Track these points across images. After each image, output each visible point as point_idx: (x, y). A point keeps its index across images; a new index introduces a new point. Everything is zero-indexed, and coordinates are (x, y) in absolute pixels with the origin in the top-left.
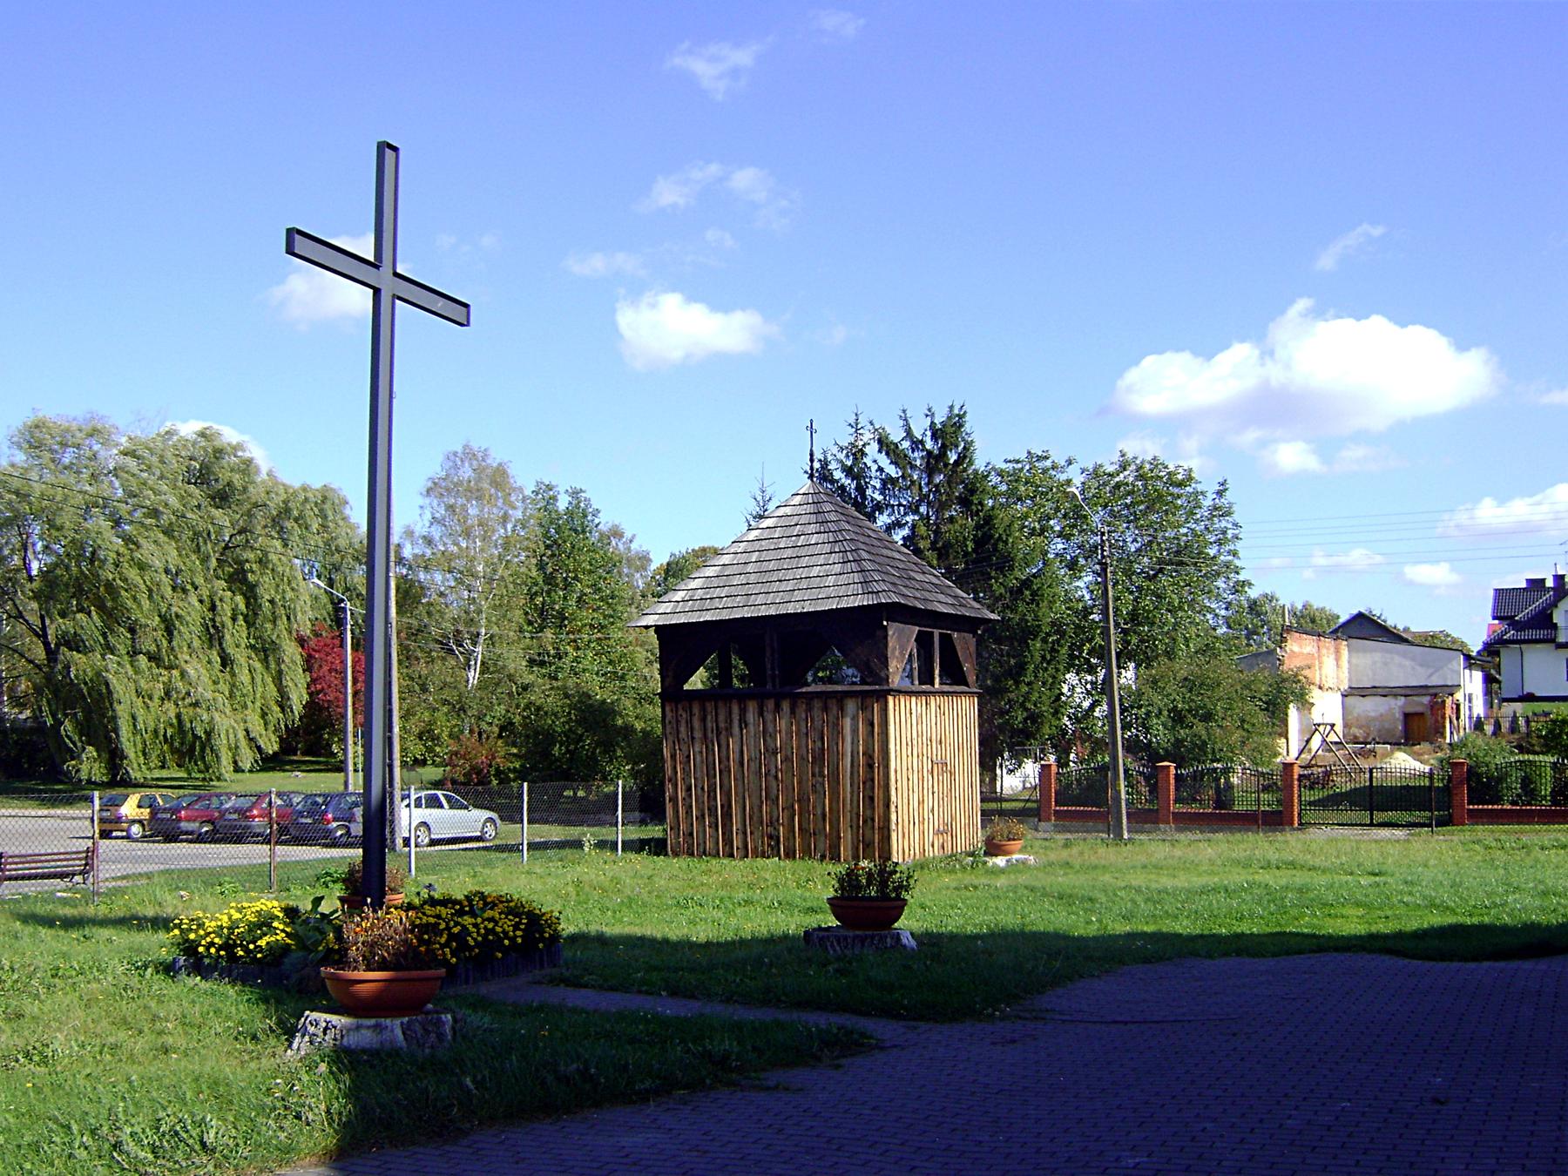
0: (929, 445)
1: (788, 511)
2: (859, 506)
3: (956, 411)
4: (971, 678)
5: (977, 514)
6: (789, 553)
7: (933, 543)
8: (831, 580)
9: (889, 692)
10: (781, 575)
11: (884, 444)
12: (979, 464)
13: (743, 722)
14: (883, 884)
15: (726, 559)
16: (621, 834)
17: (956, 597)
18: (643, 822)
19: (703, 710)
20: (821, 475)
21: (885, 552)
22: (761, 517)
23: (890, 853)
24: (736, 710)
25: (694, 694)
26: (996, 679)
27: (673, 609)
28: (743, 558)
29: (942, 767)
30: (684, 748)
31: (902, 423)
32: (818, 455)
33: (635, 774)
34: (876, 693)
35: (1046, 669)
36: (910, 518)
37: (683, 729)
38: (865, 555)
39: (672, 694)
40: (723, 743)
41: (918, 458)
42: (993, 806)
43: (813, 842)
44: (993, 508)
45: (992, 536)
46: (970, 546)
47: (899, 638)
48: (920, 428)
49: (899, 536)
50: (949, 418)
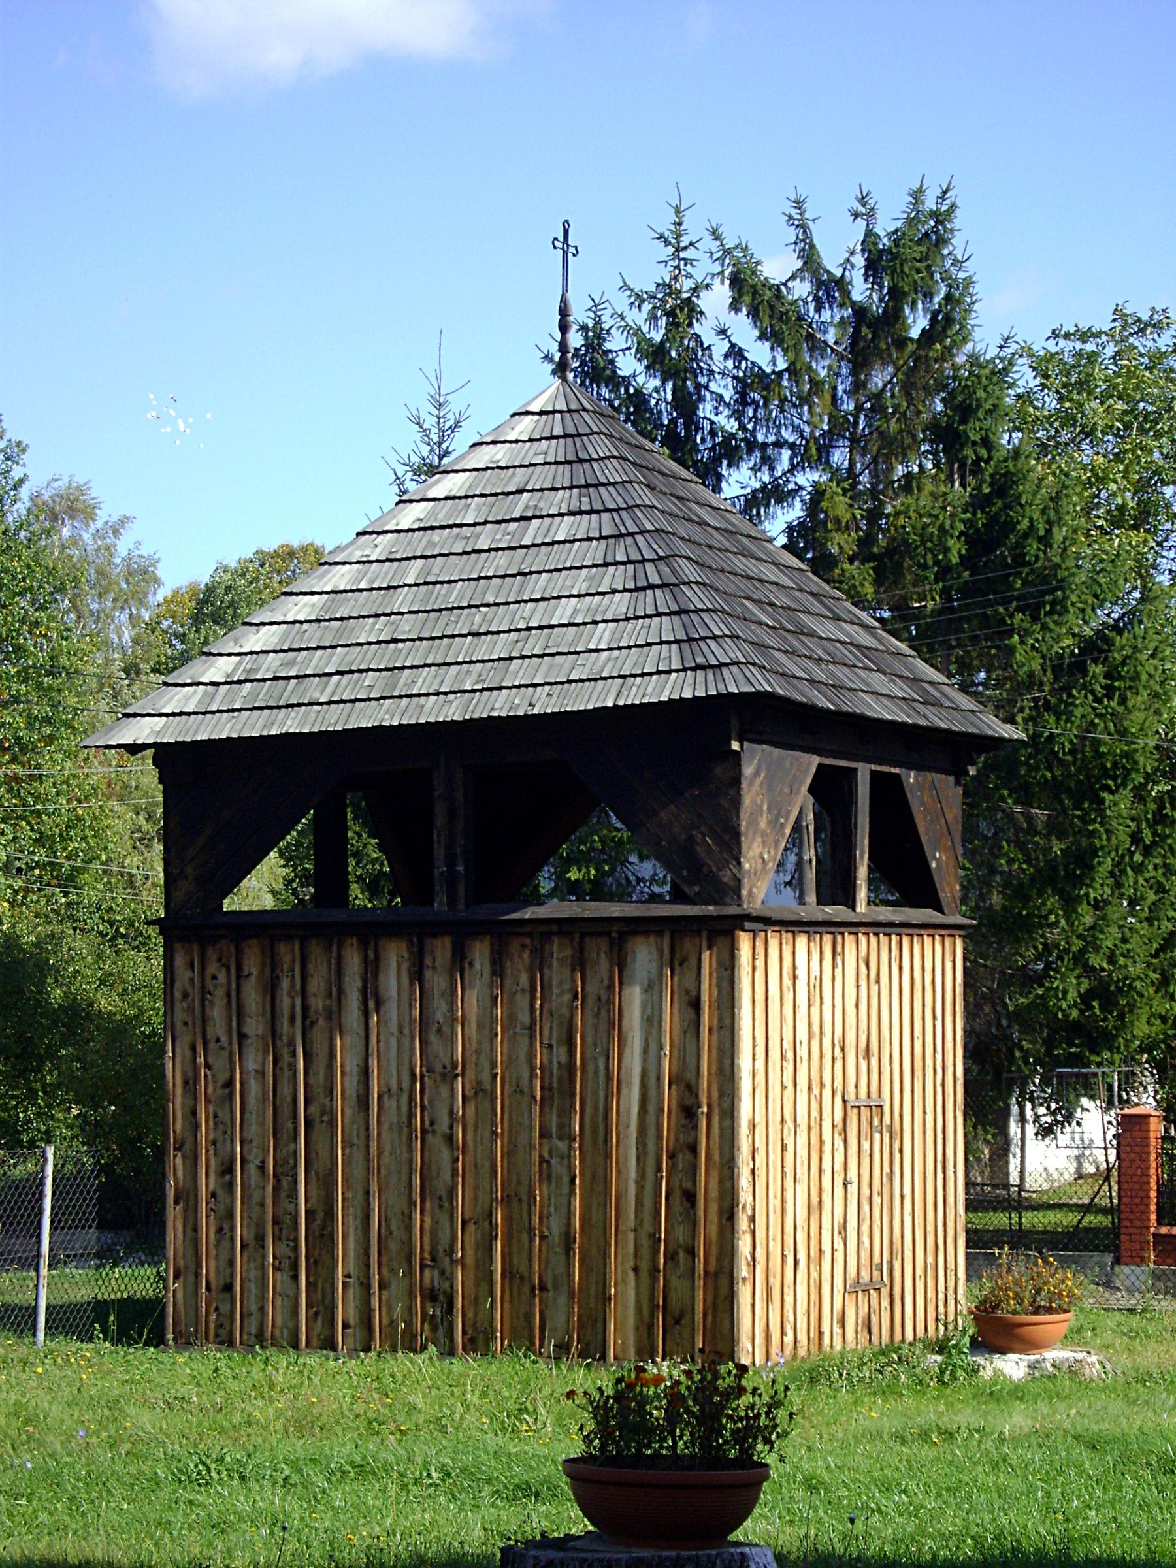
0: (860, 290)
1: (500, 454)
2: (679, 446)
3: (930, 204)
4: (949, 888)
5: (976, 470)
6: (500, 563)
7: (866, 542)
8: (602, 635)
9: (740, 921)
10: (477, 619)
11: (748, 289)
12: (985, 336)
13: (372, 997)
14: (710, 1419)
15: (340, 578)
16: (45, 1288)
17: (915, 681)
18: (106, 1256)
19: (273, 965)
20: (584, 362)
21: (741, 564)
22: (431, 470)
23: (731, 1340)
24: (353, 961)
25: (254, 925)
26: (1019, 892)
27: (182, 710)
28: (383, 575)
29: (869, 1116)
30: (219, 1062)
31: (792, 234)
32: (580, 314)
33: (91, 1131)
34: (708, 924)
35: (1139, 869)
36: (806, 479)
37: (217, 1013)
38: (690, 572)
39: (194, 921)
40: (320, 1050)
41: (830, 323)
42: (999, 1220)
43: (546, 1313)
44: (1016, 454)
45: (1010, 526)
46: (956, 549)
47: (769, 784)
49: (779, 522)
50: (910, 222)
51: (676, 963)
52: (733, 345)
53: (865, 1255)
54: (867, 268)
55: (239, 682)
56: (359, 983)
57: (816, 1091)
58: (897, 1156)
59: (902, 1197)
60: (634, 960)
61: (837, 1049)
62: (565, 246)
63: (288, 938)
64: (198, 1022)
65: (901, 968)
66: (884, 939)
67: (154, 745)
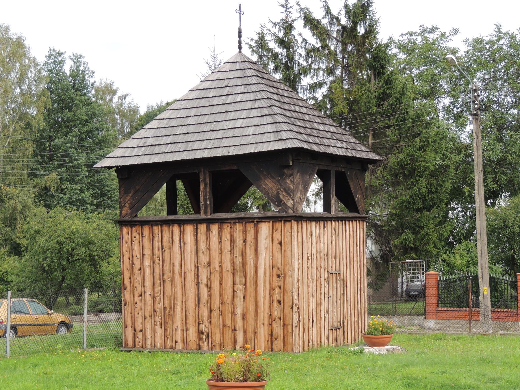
0: (344, 21)
11: (310, 22)
37: (136, 247)
41: (334, 30)
48: (337, 7)
51: (274, 231)
52: (304, 39)
53: (335, 319)
54: (346, 14)
55: (141, 147)
56: (178, 238)
57: (319, 269)
58: (345, 288)
59: (347, 301)
60: (261, 230)
61: (325, 256)
62: (240, 11)
63: (157, 225)
64: (131, 251)
65: (346, 231)
66: (337, 222)
67: (116, 166)
